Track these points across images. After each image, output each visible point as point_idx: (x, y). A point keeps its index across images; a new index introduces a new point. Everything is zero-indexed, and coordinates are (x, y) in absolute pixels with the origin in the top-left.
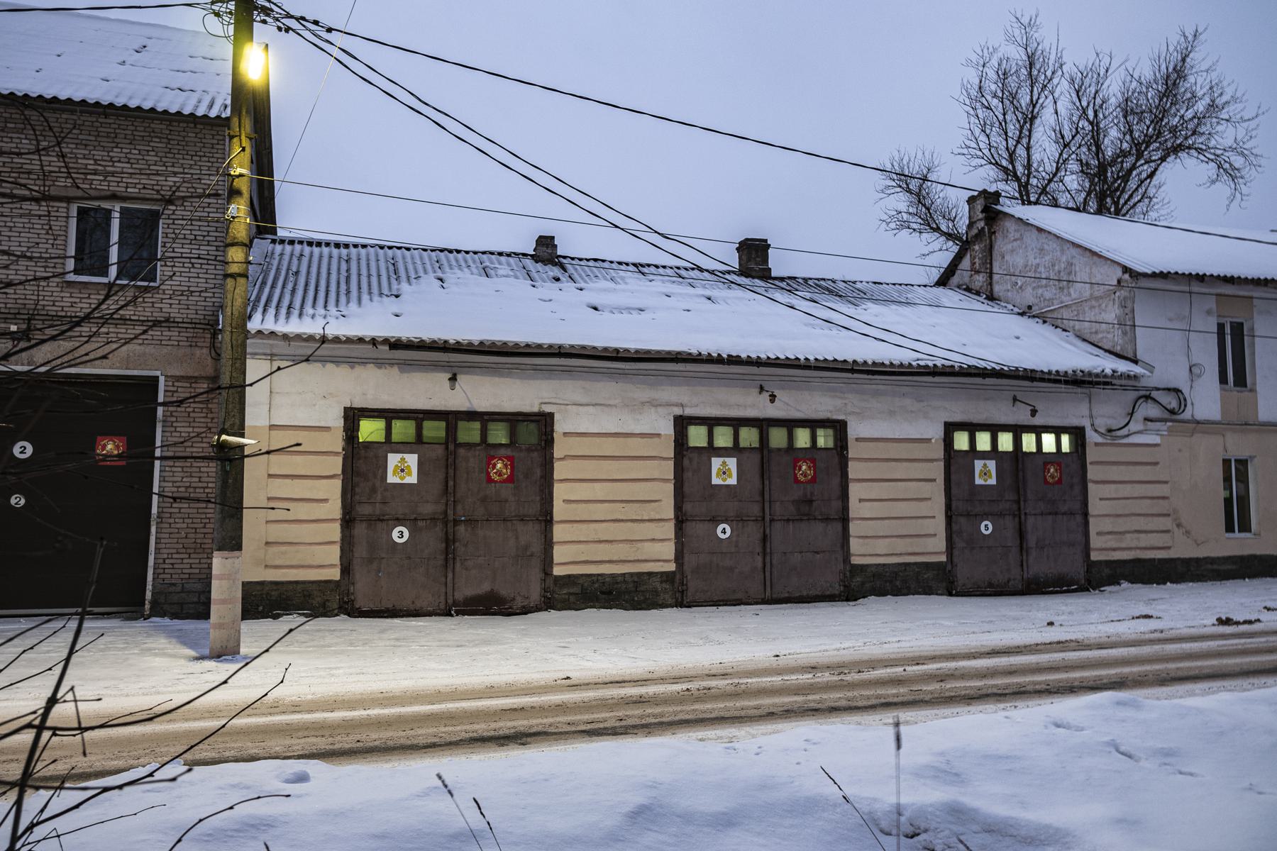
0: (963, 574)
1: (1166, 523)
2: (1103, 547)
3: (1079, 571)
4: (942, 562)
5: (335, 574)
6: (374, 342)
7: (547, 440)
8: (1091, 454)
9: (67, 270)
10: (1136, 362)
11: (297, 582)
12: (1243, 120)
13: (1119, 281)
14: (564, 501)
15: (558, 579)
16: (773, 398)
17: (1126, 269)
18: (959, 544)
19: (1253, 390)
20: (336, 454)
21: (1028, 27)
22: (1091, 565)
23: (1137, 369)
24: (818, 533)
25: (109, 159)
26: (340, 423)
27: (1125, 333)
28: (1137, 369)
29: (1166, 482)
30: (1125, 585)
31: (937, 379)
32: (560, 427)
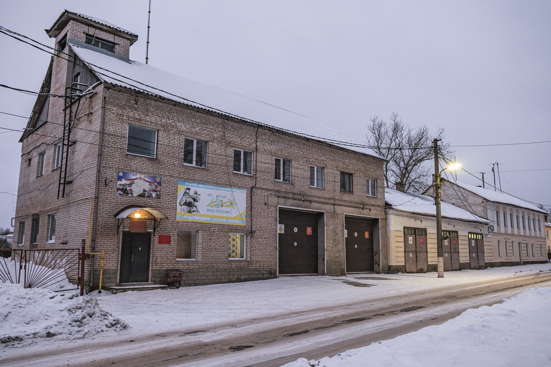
0: (472, 265)
1: (492, 255)
2: (487, 260)
3: (425, 268)
4: (518, 262)
5: (403, 264)
6: (410, 213)
7: (426, 234)
8: (484, 239)
9: (443, 205)
10: (488, 220)
11: (399, 266)
12: (451, 152)
13: (482, 202)
14: (84, 240)
15: (429, 265)
16: (454, 226)
17: (484, 199)
18: (471, 259)
19: (507, 227)
20: (467, 240)
21: (396, 116)
22: (390, 267)
23: (488, 221)
24: (456, 254)
25: (162, 116)
26: (402, 230)
27: (484, 213)
28: (488, 221)
29: (491, 246)
30: (489, 268)
31: (471, 223)
32: (428, 231)
